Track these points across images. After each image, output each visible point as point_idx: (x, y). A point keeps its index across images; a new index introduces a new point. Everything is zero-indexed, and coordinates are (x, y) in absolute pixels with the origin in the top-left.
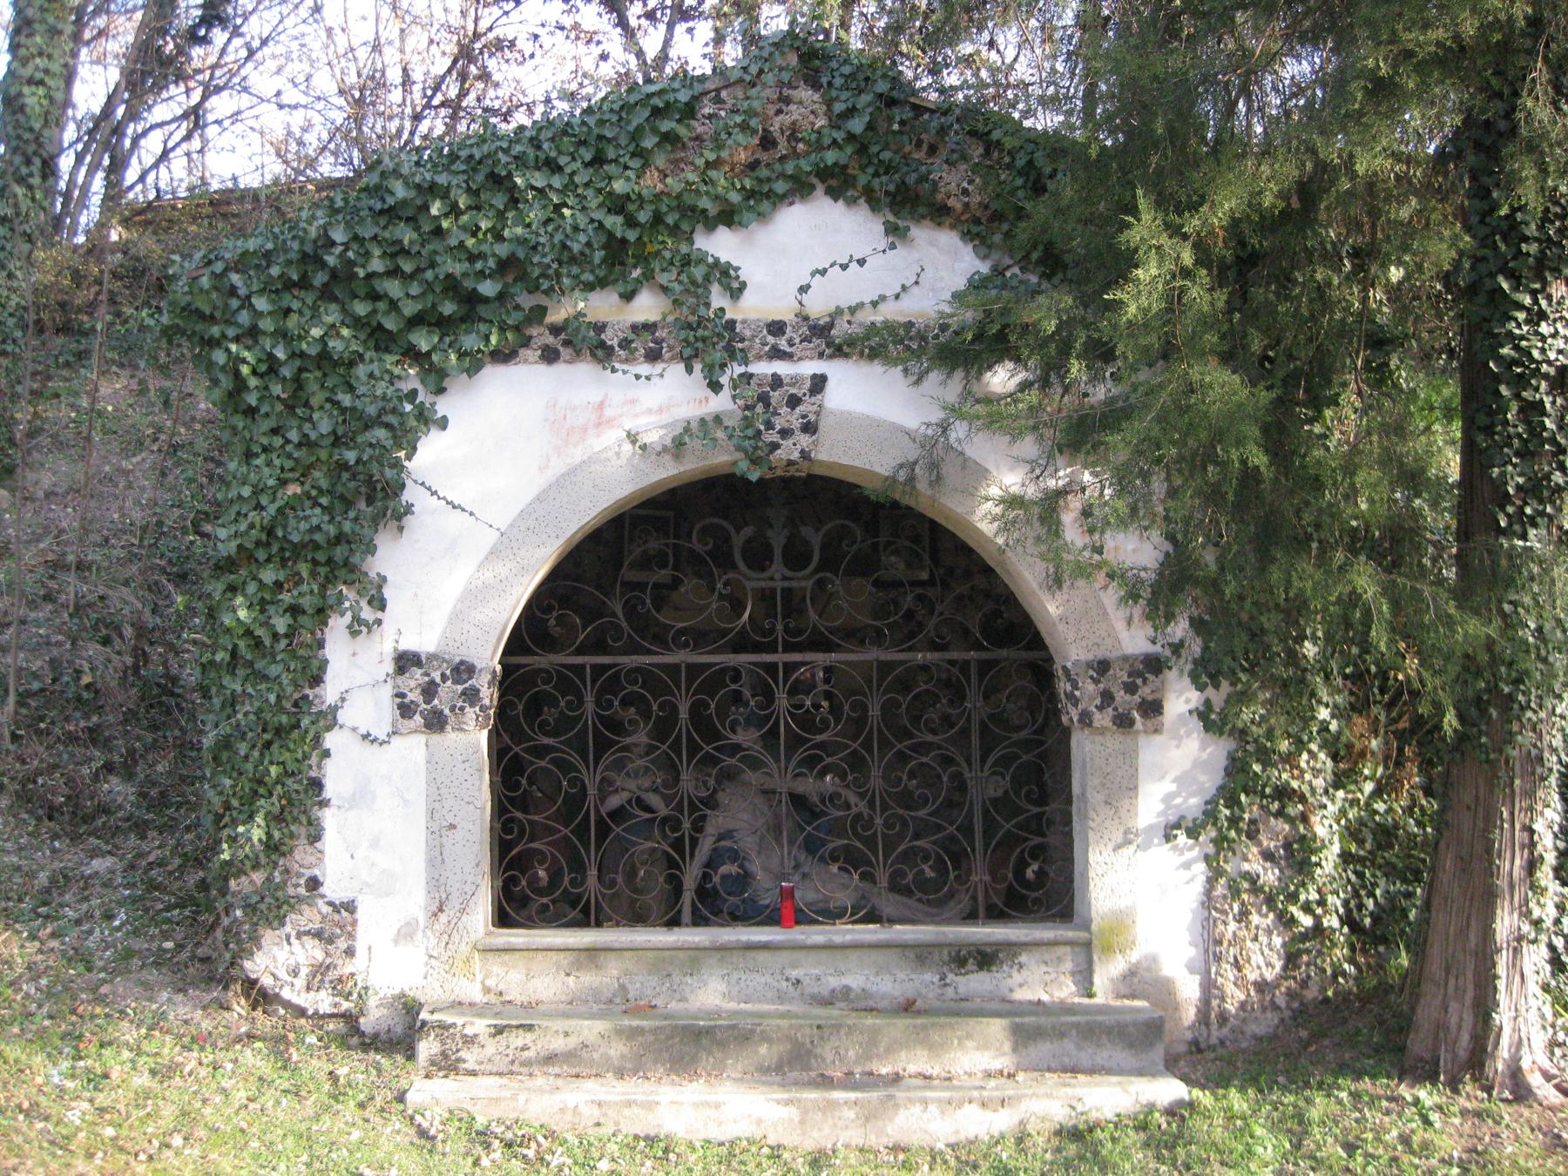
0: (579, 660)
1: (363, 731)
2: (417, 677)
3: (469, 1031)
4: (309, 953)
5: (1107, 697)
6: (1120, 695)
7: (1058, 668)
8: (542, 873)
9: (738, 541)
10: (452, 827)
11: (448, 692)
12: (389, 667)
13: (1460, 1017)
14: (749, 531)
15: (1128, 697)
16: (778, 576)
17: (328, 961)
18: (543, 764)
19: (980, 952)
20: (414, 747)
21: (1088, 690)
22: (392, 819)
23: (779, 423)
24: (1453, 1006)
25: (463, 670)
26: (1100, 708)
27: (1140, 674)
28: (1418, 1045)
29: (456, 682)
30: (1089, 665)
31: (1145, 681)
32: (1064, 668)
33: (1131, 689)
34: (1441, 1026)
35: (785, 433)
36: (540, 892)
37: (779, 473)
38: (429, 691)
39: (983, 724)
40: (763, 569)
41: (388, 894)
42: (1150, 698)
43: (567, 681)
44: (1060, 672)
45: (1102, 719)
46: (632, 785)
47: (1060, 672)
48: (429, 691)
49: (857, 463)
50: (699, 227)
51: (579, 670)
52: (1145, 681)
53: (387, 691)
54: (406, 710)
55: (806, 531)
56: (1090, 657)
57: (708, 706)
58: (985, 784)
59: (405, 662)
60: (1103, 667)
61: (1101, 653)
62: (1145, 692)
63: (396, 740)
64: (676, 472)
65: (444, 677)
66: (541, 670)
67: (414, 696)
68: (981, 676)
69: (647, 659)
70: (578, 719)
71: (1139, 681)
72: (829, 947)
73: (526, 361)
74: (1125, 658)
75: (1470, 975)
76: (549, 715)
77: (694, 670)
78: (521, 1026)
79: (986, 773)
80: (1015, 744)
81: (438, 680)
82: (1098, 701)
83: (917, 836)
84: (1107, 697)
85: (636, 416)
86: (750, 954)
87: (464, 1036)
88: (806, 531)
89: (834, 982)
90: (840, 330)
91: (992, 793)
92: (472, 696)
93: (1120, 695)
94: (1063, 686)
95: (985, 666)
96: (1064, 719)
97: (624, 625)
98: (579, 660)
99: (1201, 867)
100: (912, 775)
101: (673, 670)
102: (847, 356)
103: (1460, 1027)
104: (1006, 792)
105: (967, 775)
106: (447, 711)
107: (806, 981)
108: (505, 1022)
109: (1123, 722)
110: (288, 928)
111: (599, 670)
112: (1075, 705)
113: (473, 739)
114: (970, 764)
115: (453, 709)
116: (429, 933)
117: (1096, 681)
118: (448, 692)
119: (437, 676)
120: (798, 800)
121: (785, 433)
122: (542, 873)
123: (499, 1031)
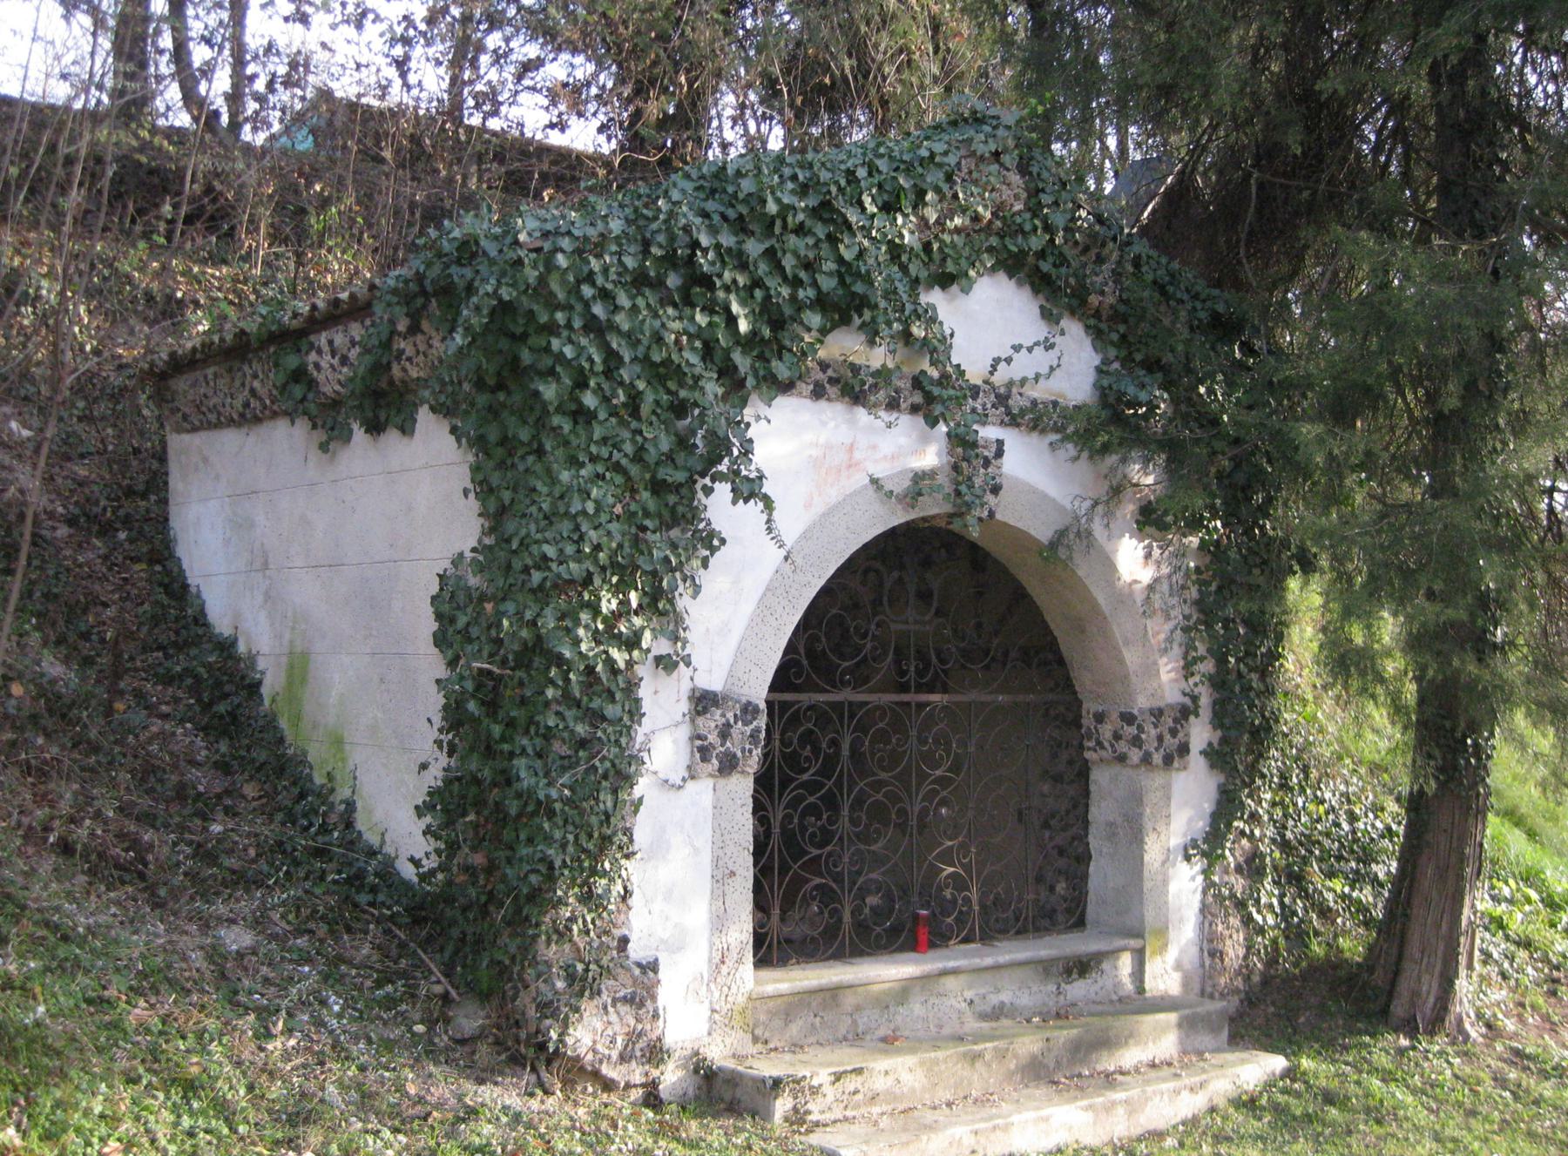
1: (662, 776)
2: (716, 717)
3: (815, 1082)
4: (621, 1022)
10: (733, 874)
12: (684, 706)
13: (1429, 987)
16: (911, 620)
17: (640, 1027)
19: (1081, 962)
20: (702, 792)
22: (678, 873)
24: (1425, 978)
28: (1399, 1009)
29: (746, 724)
34: (1415, 994)
38: (725, 732)
49: (1019, 525)
50: (1066, 314)
53: (685, 731)
54: (704, 752)
59: (703, 702)
63: (690, 785)
64: (902, 520)
67: (713, 738)
69: (821, 697)
72: (997, 967)
73: (800, 394)
75: (1440, 954)
78: (854, 1070)
83: (820, 856)
85: (876, 461)
87: (811, 1087)
89: (994, 999)
90: (1016, 402)
97: (805, 662)
99: (1200, 878)
102: (1018, 425)
103: (1429, 993)
106: (739, 754)
107: (977, 1000)
108: (842, 1069)
110: (605, 997)
113: (742, 787)
115: (743, 750)
116: (712, 986)
119: (730, 716)
123: (838, 1077)
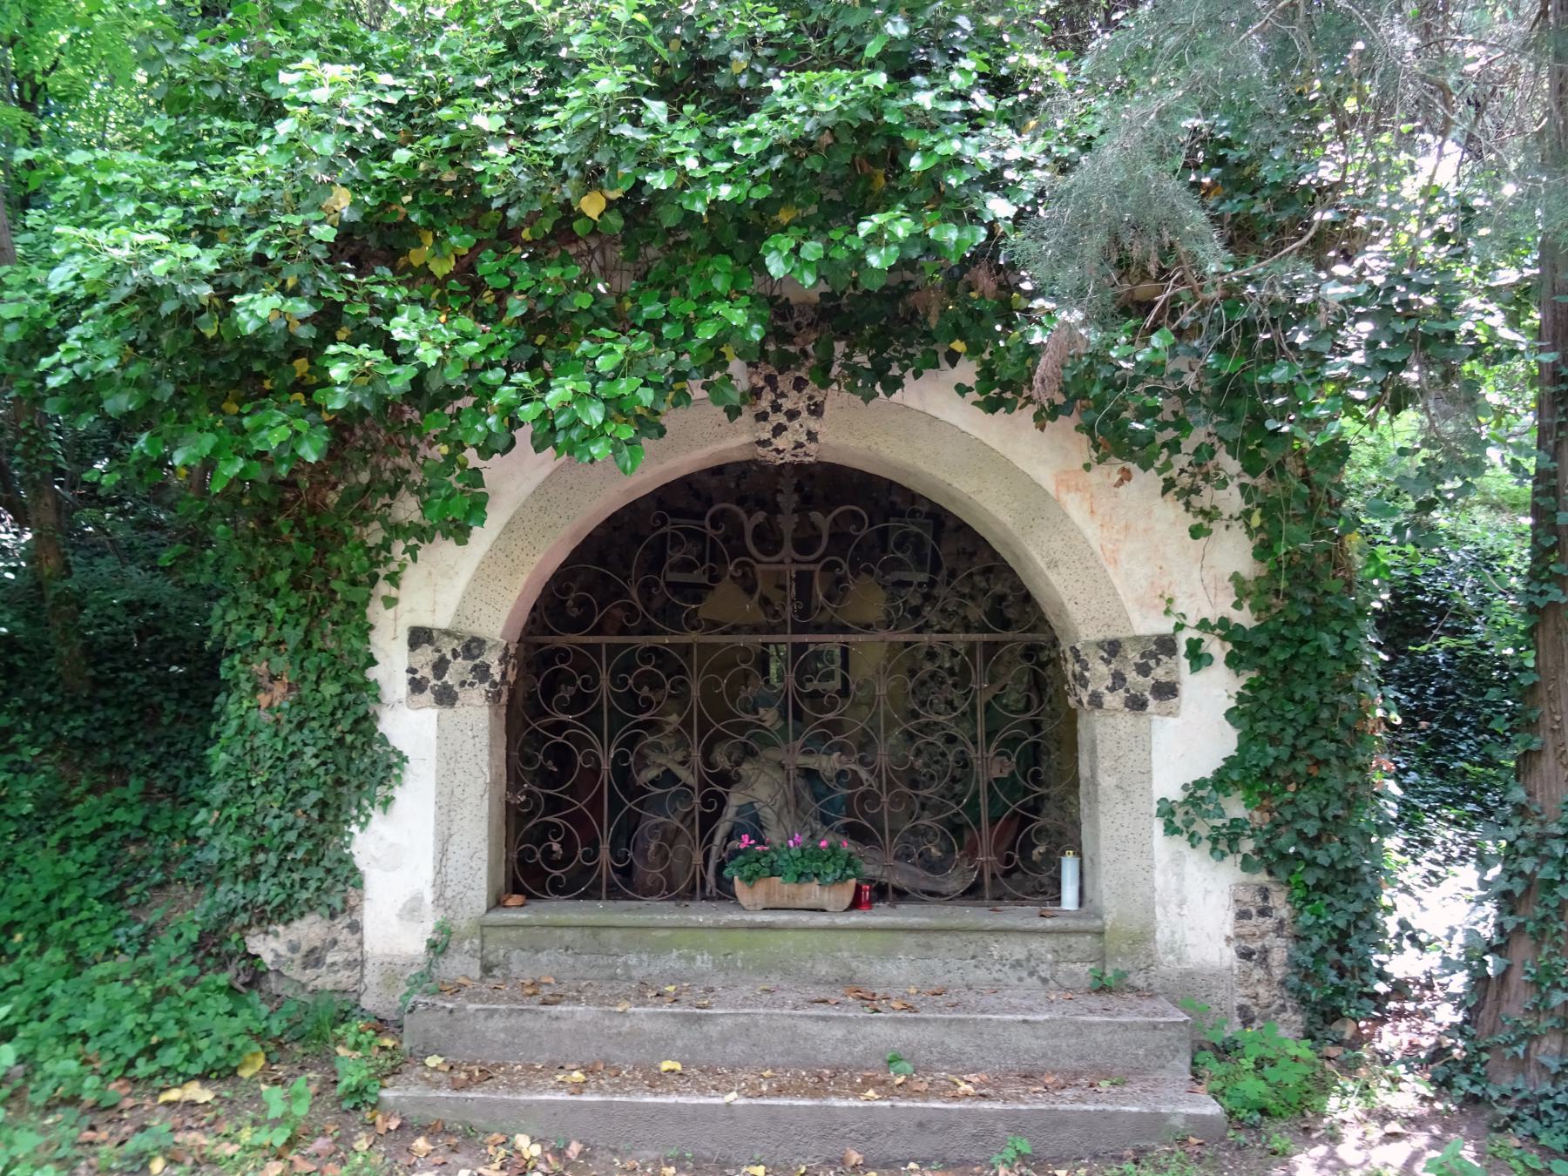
0: (591, 640)
5: (1119, 679)
6: (1132, 676)
7: (1065, 646)
8: (556, 847)
9: (749, 528)
11: (458, 669)
14: (760, 516)
15: (1140, 679)
18: (560, 739)
21: (1100, 672)
23: (787, 404)
25: (472, 647)
26: (1112, 689)
27: (1153, 655)
30: (1100, 645)
31: (1158, 662)
32: (1073, 649)
33: (1144, 670)
35: (793, 415)
36: (555, 865)
37: (788, 458)
38: (440, 667)
39: (988, 706)
40: (776, 552)
41: (394, 868)
42: (1163, 679)
43: (585, 662)
44: (1068, 654)
45: (1113, 700)
46: (662, 760)
47: (1068, 654)
48: (440, 667)
51: (594, 649)
52: (1158, 662)
55: (816, 516)
56: (1100, 637)
57: (718, 685)
58: (992, 766)
60: (1113, 648)
61: (1111, 635)
62: (1159, 673)
65: (455, 654)
66: (559, 649)
67: (426, 672)
68: (987, 660)
70: (593, 696)
71: (1152, 663)
74: (1137, 639)
76: (567, 692)
77: (706, 649)
79: (992, 753)
80: (823, 725)
81: (449, 657)
82: (1109, 682)
84: (1119, 679)
86: (756, 933)
88: (816, 516)
91: (996, 773)
92: (482, 672)
93: (1132, 676)
94: (1071, 667)
95: (990, 648)
96: (1071, 701)
98: (591, 640)
100: (918, 753)
101: (686, 649)
104: (1012, 774)
105: (973, 755)
109: (1136, 704)
111: (613, 649)
112: (1085, 686)
114: (975, 743)
117: (1108, 662)
118: (458, 669)
120: (810, 774)
121: (793, 415)
122: (556, 847)
